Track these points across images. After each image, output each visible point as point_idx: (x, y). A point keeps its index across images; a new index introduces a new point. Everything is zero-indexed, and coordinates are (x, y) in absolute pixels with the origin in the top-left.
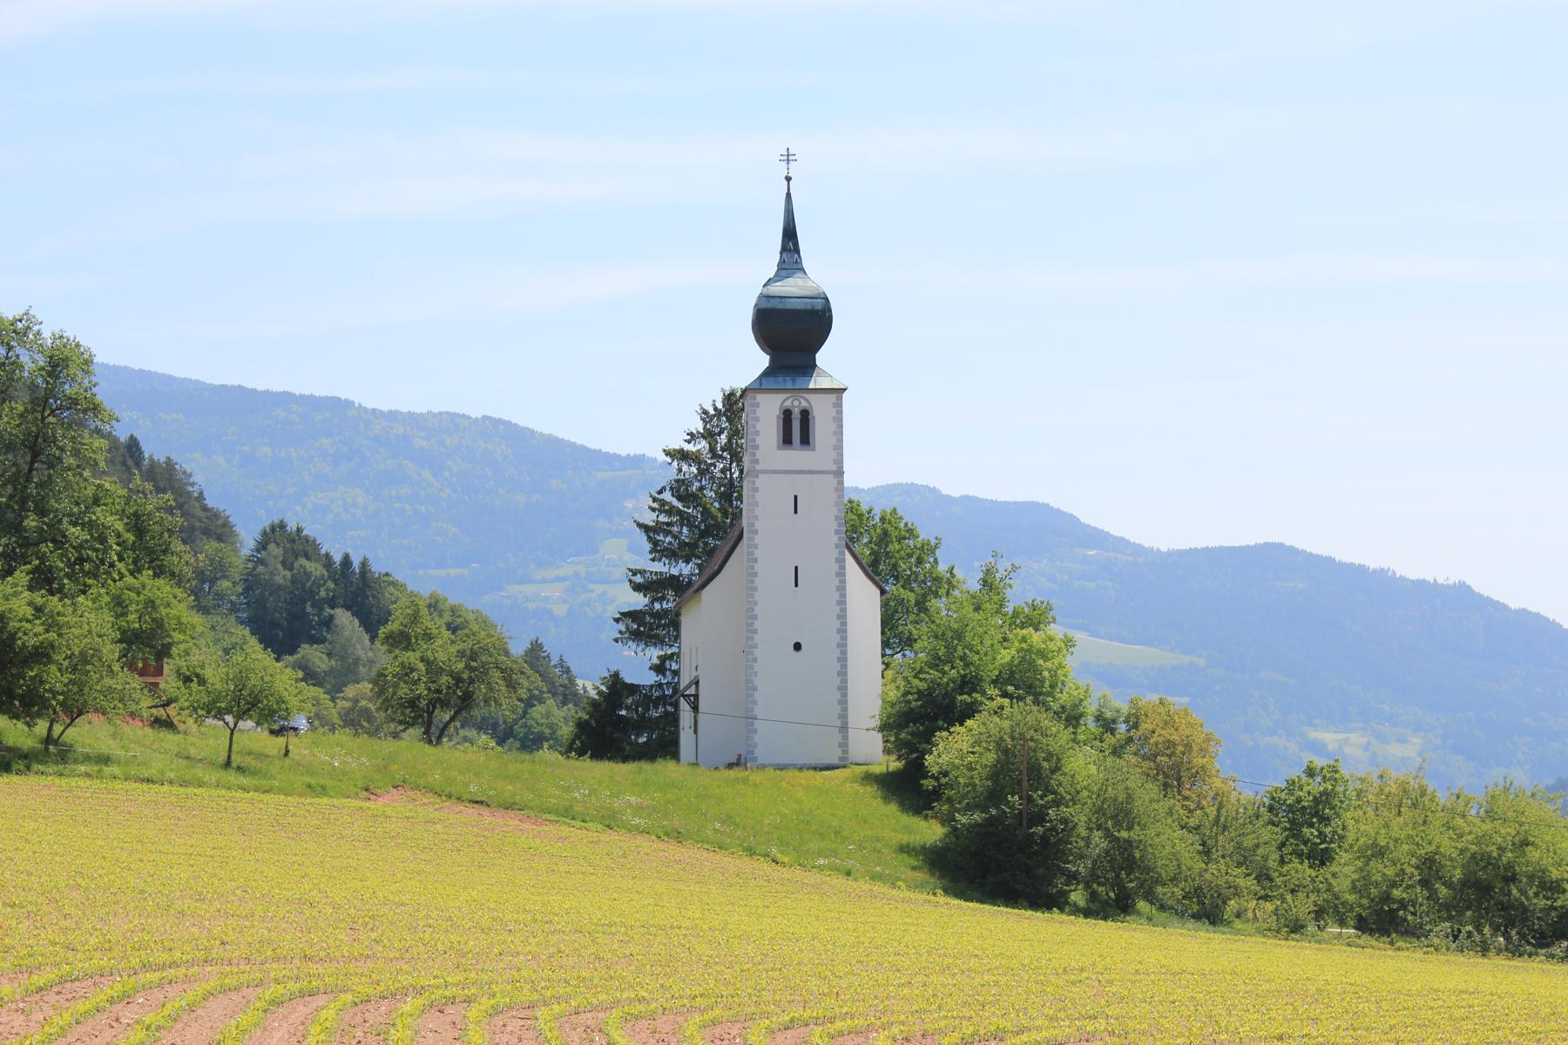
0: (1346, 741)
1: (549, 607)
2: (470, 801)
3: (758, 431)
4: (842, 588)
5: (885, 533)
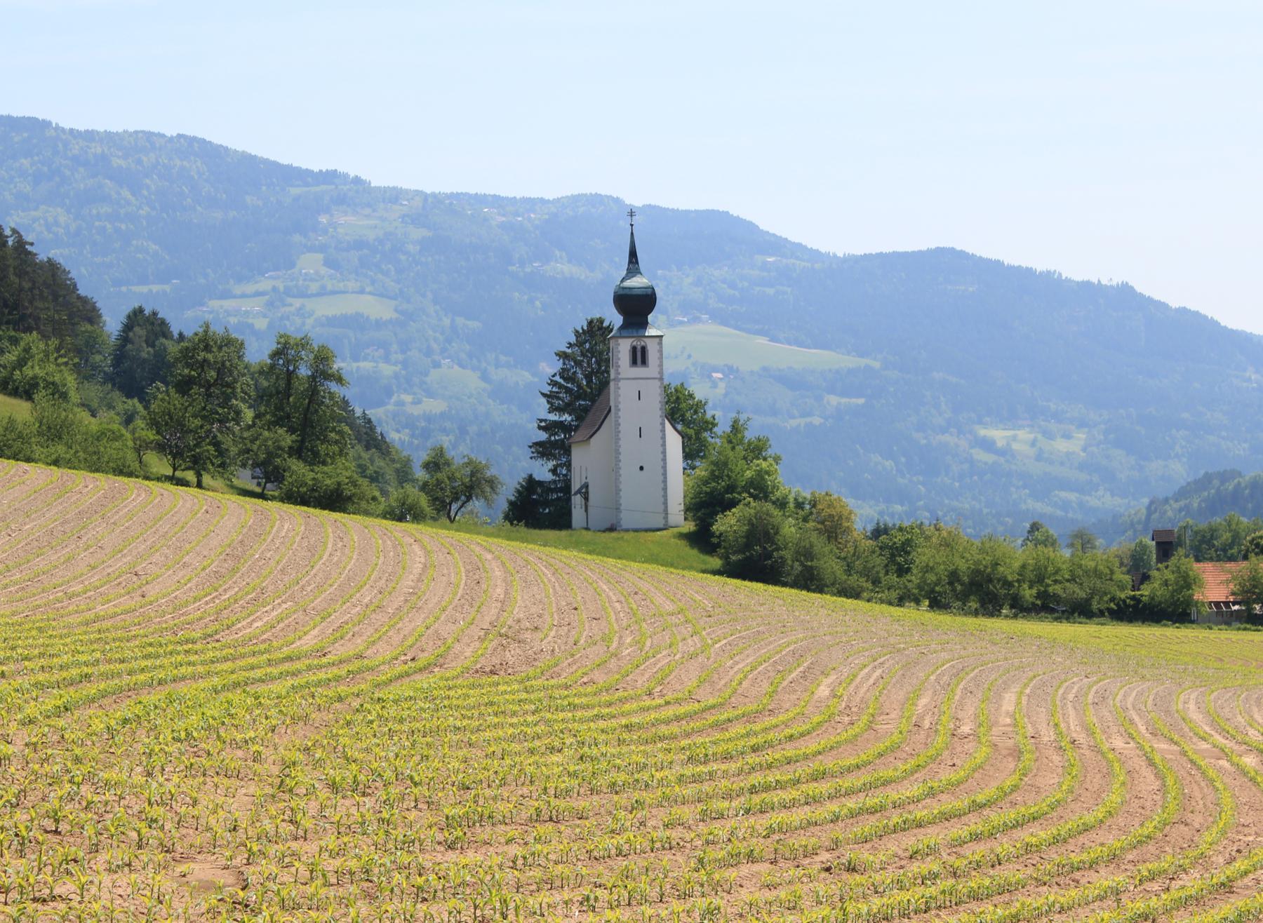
0: (1014, 438)
1: (250, 321)
4: (664, 438)
5: (678, 398)
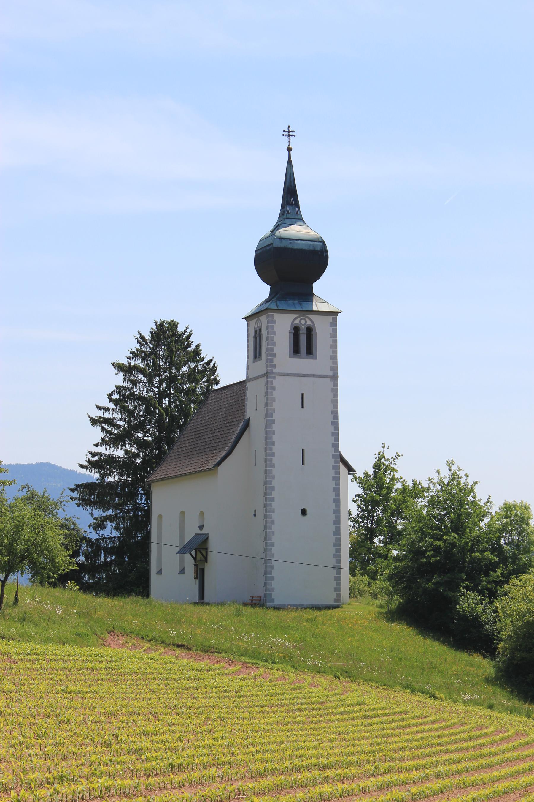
2: (174, 645)
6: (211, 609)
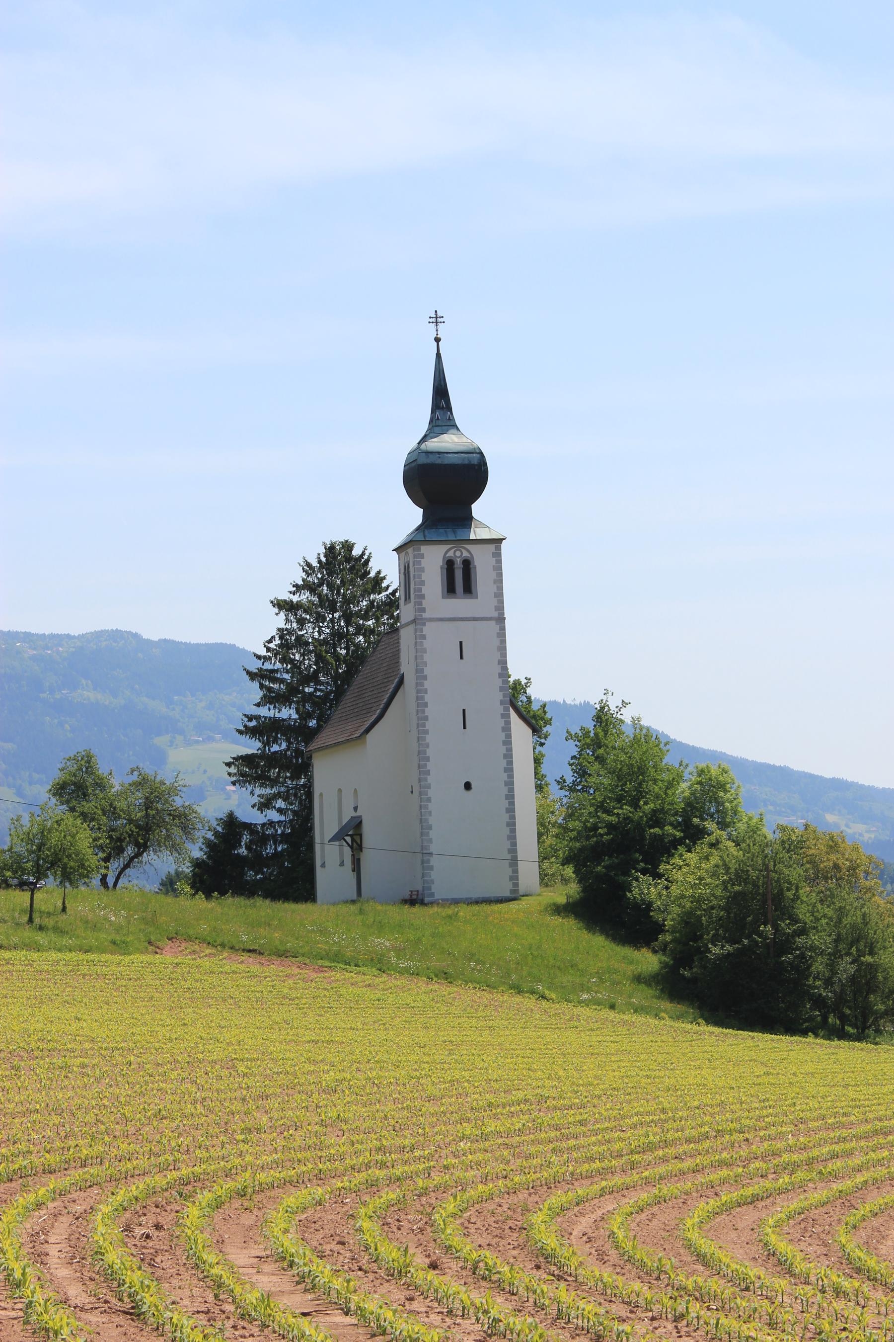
2: (244, 950)
3: (424, 581)
6: (329, 909)
